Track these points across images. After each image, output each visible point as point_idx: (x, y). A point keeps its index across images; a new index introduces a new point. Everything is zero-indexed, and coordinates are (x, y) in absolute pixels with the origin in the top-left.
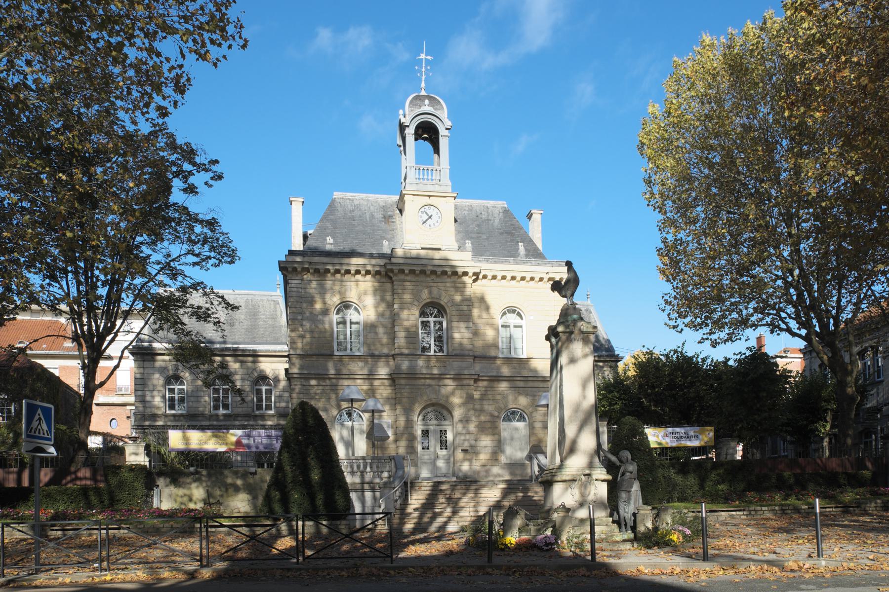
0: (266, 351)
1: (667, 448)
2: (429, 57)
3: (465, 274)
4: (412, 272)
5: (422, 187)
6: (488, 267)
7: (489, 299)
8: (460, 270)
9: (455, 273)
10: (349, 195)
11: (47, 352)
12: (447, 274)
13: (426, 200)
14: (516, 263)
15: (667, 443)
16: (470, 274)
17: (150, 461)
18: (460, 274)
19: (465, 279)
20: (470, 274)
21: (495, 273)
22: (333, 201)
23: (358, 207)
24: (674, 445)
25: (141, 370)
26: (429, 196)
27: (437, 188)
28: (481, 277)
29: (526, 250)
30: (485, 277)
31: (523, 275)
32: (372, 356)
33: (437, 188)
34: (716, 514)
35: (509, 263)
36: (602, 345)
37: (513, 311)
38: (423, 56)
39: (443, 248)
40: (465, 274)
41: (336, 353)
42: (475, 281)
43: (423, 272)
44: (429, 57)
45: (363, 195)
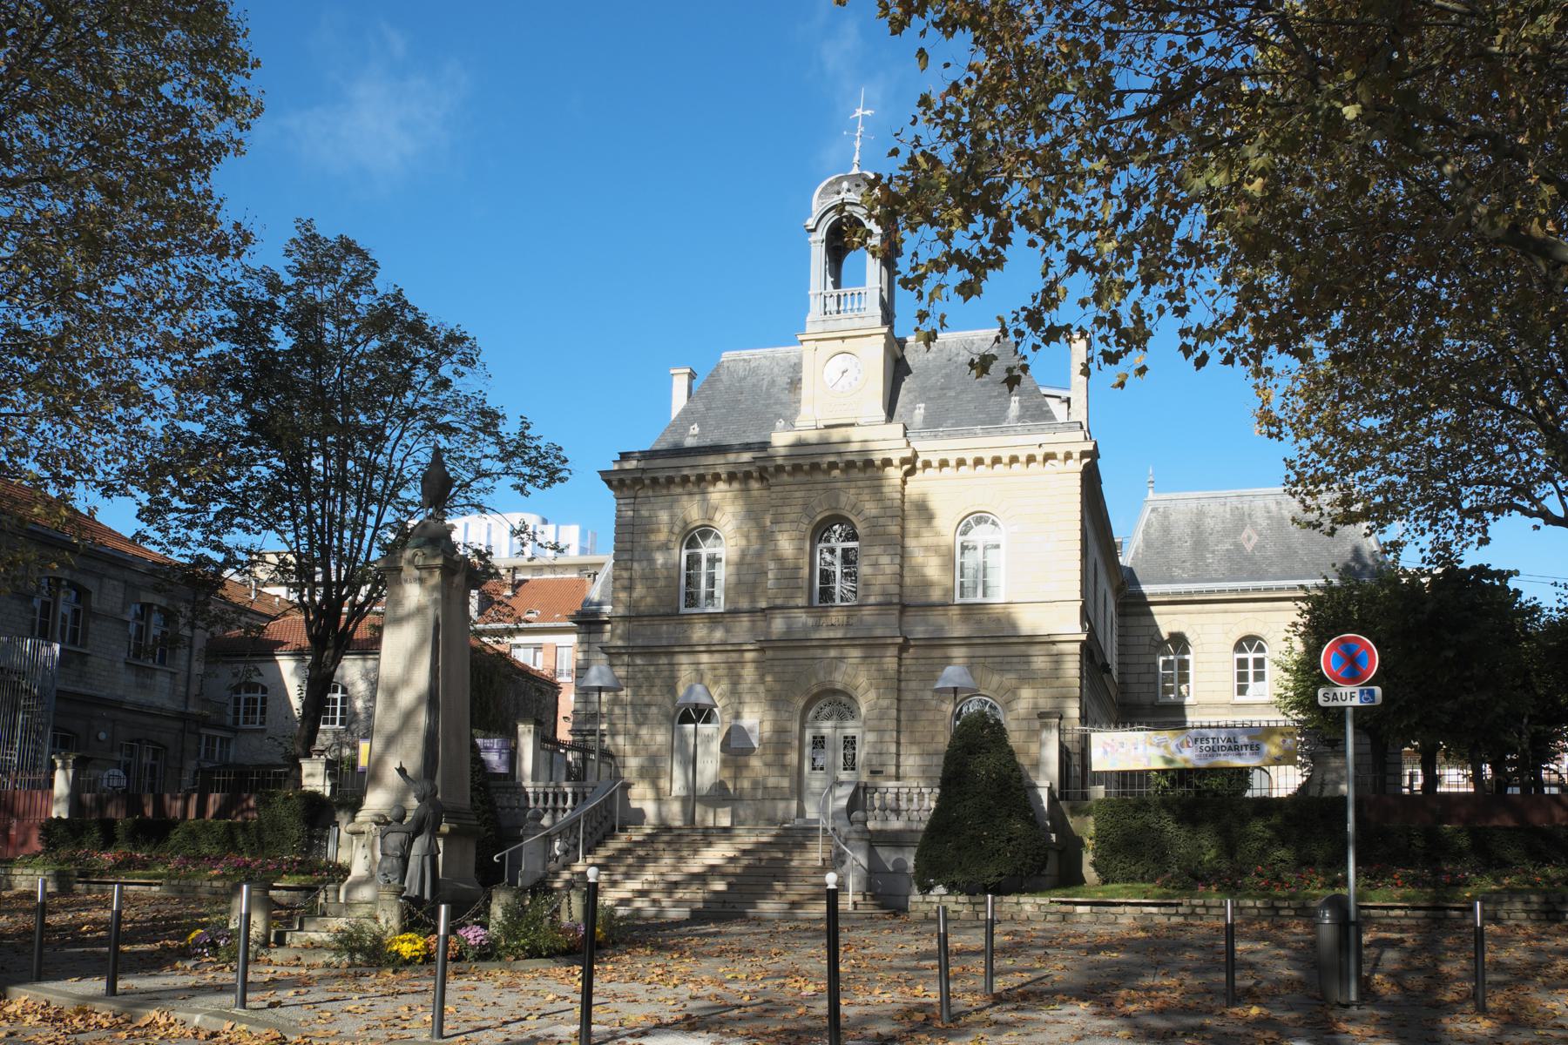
0: (1162, 594)
1: (1189, 771)
2: (868, 112)
3: (887, 462)
4: (797, 468)
5: (831, 325)
6: (929, 448)
7: (935, 504)
8: (878, 458)
9: (869, 463)
10: (745, 354)
11: (542, 625)
12: (867, 467)
13: (838, 345)
14: (1003, 432)
15: (1186, 761)
16: (896, 462)
17: (333, 786)
18: (878, 463)
19: (890, 471)
20: (896, 462)
21: (944, 456)
22: (719, 366)
23: (754, 371)
24: (1203, 764)
25: (585, 647)
26: (843, 338)
27: (857, 323)
28: (919, 464)
29: (1022, 407)
30: (927, 464)
31: (996, 453)
32: (904, 608)
33: (857, 323)
34: (1113, 909)
35: (975, 435)
36: (1365, 566)
37: (979, 521)
38: (859, 112)
39: (861, 422)
40: (887, 462)
41: (683, 610)
42: (908, 473)
43: (815, 467)
44: (868, 112)
45: (767, 351)
